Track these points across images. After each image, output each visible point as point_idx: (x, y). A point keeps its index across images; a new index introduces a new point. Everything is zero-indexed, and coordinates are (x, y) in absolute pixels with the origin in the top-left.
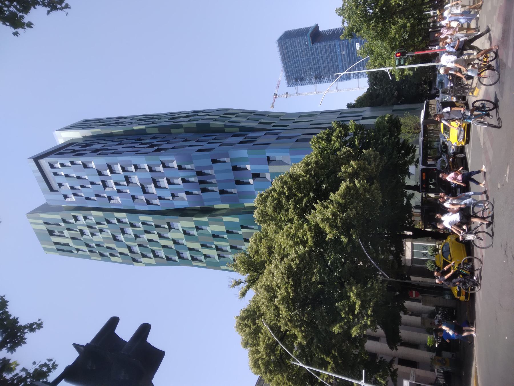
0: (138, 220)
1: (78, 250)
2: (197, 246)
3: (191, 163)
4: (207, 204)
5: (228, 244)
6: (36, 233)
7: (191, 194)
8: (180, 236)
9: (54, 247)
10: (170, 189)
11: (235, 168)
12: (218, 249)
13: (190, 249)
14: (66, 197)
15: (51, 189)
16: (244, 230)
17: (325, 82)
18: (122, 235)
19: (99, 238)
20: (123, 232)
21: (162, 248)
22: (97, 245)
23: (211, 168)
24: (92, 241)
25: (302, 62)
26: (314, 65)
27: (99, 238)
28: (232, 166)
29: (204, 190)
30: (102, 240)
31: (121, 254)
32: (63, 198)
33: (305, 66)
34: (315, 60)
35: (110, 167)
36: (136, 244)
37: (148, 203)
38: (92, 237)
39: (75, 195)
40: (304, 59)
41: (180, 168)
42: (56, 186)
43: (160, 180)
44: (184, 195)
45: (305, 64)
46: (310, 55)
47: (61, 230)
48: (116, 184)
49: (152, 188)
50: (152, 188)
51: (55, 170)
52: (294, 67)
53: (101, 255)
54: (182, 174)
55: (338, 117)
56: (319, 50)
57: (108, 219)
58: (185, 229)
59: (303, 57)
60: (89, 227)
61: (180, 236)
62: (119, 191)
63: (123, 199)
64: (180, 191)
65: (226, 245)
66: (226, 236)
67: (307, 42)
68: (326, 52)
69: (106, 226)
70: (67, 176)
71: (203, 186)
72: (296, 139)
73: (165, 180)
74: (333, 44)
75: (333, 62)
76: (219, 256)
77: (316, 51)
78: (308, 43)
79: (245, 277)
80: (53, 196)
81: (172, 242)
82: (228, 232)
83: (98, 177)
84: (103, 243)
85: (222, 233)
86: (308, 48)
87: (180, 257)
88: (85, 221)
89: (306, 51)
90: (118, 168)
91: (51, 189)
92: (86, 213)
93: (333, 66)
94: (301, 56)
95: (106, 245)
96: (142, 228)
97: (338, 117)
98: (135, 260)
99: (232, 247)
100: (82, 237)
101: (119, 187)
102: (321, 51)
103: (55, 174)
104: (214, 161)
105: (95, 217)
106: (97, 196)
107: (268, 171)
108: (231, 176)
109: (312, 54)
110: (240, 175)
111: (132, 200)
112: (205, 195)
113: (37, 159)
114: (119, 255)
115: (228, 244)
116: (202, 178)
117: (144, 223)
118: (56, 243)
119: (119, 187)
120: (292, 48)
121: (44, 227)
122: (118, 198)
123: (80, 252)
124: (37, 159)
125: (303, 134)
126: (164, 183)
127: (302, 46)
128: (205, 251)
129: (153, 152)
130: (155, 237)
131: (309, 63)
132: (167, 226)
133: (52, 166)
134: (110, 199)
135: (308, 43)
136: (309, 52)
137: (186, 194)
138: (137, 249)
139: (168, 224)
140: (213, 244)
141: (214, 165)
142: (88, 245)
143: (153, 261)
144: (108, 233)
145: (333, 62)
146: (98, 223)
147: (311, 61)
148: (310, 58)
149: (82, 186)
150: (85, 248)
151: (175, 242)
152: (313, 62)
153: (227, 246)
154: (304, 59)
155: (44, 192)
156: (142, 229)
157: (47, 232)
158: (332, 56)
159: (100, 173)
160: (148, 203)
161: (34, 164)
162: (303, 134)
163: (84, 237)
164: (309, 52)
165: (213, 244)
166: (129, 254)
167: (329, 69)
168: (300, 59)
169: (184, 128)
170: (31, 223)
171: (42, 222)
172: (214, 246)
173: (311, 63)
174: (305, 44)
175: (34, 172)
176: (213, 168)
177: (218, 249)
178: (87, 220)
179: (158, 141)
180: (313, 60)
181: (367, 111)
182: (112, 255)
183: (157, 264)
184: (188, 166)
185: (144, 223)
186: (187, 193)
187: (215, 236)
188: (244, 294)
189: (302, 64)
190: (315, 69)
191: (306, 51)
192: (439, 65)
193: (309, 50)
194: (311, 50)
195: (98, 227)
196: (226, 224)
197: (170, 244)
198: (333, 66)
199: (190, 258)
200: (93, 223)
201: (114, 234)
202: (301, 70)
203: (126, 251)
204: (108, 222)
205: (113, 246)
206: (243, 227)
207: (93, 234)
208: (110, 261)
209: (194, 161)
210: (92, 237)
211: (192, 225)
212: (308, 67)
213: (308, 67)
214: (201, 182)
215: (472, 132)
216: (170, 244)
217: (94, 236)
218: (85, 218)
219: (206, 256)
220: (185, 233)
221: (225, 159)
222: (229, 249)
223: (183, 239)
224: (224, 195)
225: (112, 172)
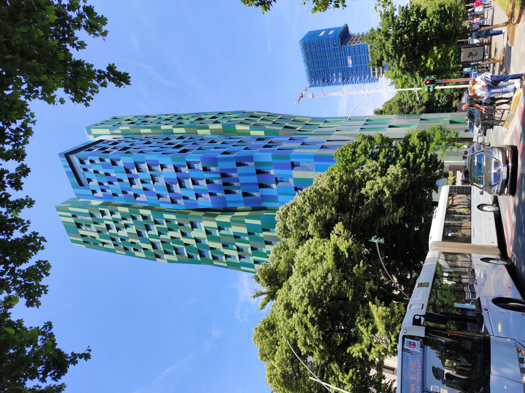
0: (163, 218)
1: (104, 243)
2: (218, 246)
3: (216, 166)
4: (229, 205)
5: (249, 246)
6: (64, 225)
7: (215, 195)
8: (202, 235)
9: (81, 240)
10: (195, 190)
11: (259, 172)
12: (239, 249)
13: (211, 248)
14: (94, 192)
15: (81, 184)
16: (265, 233)
17: (353, 83)
18: (146, 231)
19: (123, 233)
20: (148, 228)
21: (184, 246)
22: (122, 240)
23: (235, 171)
24: (117, 235)
25: (330, 62)
26: (342, 65)
27: (123, 233)
28: (256, 170)
29: (227, 192)
30: (127, 236)
31: (144, 249)
32: (91, 194)
33: (333, 66)
34: (343, 61)
35: (136, 165)
36: (159, 241)
37: (173, 201)
38: (118, 232)
39: (103, 190)
40: (331, 60)
41: (205, 169)
42: (84, 181)
43: (185, 181)
44: (208, 196)
45: (332, 64)
46: (338, 55)
47: (88, 224)
48: (142, 182)
49: (176, 188)
50: (176, 188)
51: (84, 166)
52: (321, 67)
53: (126, 249)
54: (207, 175)
55: (365, 124)
56: (348, 51)
57: (133, 215)
58: (208, 229)
59: (331, 58)
60: (115, 222)
61: (202, 235)
62: (144, 189)
63: (148, 197)
64: (205, 192)
65: (247, 247)
66: (247, 238)
67: (336, 43)
68: (355, 53)
69: (130, 221)
70: (96, 172)
71: (227, 188)
72: (321, 145)
73: (190, 180)
74: (363, 56)
75: (361, 63)
76: (240, 257)
77: (345, 52)
78: (336, 44)
79: (265, 289)
80: (82, 191)
81: (194, 241)
82: (249, 233)
83: (126, 174)
84: (128, 238)
85: (244, 235)
86: (337, 48)
87: (201, 256)
88: (111, 216)
89: (335, 51)
90: (145, 167)
91: (81, 184)
92: (113, 208)
93: (362, 67)
94: (329, 56)
95: (130, 240)
96: (165, 225)
97: (365, 124)
98: (157, 256)
99: (253, 249)
100: (108, 231)
101: (145, 186)
102: (350, 51)
103: (85, 170)
104: (239, 164)
105: (122, 213)
106: (124, 192)
107: (291, 176)
108: (254, 179)
109: (340, 55)
110: (264, 180)
111: (157, 198)
112: (228, 197)
113: (67, 155)
114: (142, 250)
115: (249, 246)
116: (226, 180)
117: (167, 221)
118: (83, 236)
119: (145, 186)
120: (322, 59)
121: (72, 220)
122: (144, 196)
123: (105, 246)
124: (67, 155)
125: (328, 141)
126: (188, 183)
127: (331, 46)
128: (227, 252)
129: (179, 152)
130: (177, 234)
131: (337, 64)
132: (190, 226)
133: (82, 162)
134: (136, 196)
135: (336, 44)
136: (337, 53)
137: (210, 195)
138: (161, 246)
139: (192, 223)
140: (235, 245)
141: (239, 168)
142: (113, 239)
143: (174, 257)
144: (133, 230)
145: (361, 63)
146: (123, 219)
147: (339, 61)
148: (338, 59)
149: (110, 183)
150: (110, 242)
151: (197, 241)
152: (341, 63)
153: (248, 247)
154: (331, 60)
155: (74, 187)
156: (166, 227)
157: (75, 225)
158: (360, 57)
159: (127, 171)
160: (173, 201)
161: (65, 159)
162: (328, 141)
163: (110, 231)
164: (337, 53)
165: (235, 245)
166: (152, 250)
167: (357, 70)
168: (328, 59)
169: (211, 130)
170: (73, 241)
171: (70, 215)
172: (235, 247)
173: (339, 63)
174: (334, 44)
175: (65, 166)
176: (238, 171)
177: (239, 249)
178: (113, 215)
179: (184, 142)
180: (341, 61)
181: (394, 119)
182: (135, 250)
183: (179, 261)
184: (213, 169)
185: (167, 221)
186: (211, 194)
187: (236, 237)
188: (264, 305)
189: (330, 64)
190: (342, 69)
191: (335, 51)
192: (474, 122)
193: (337, 51)
194: (340, 50)
195: (123, 222)
196: (248, 226)
197: (193, 242)
198: (362, 67)
199: (211, 258)
200: (119, 219)
201: (139, 230)
202: (329, 71)
203: (149, 247)
204: (134, 218)
205: (137, 241)
206: (264, 230)
207: (118, 229)
208: (133, 255)
209: (218, 163)
210: (118, 232)
211: (215, 225)
212: (336, 67)
213: (336, 67)
214: (225, 184)
215: (503, 208)
216: (193, 242)
217: (119, 231)
218: (112, 213)
219: (227, 256)
220: (208, 232)
221: (249, 163)
222: (250, 251)
223: (204, 239)
224: (247, 198)
225: (139, 170)
